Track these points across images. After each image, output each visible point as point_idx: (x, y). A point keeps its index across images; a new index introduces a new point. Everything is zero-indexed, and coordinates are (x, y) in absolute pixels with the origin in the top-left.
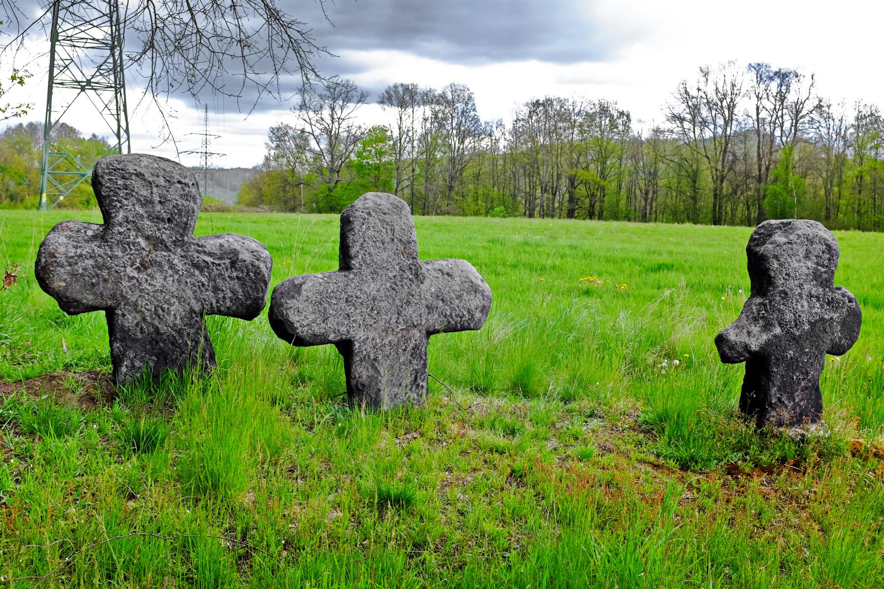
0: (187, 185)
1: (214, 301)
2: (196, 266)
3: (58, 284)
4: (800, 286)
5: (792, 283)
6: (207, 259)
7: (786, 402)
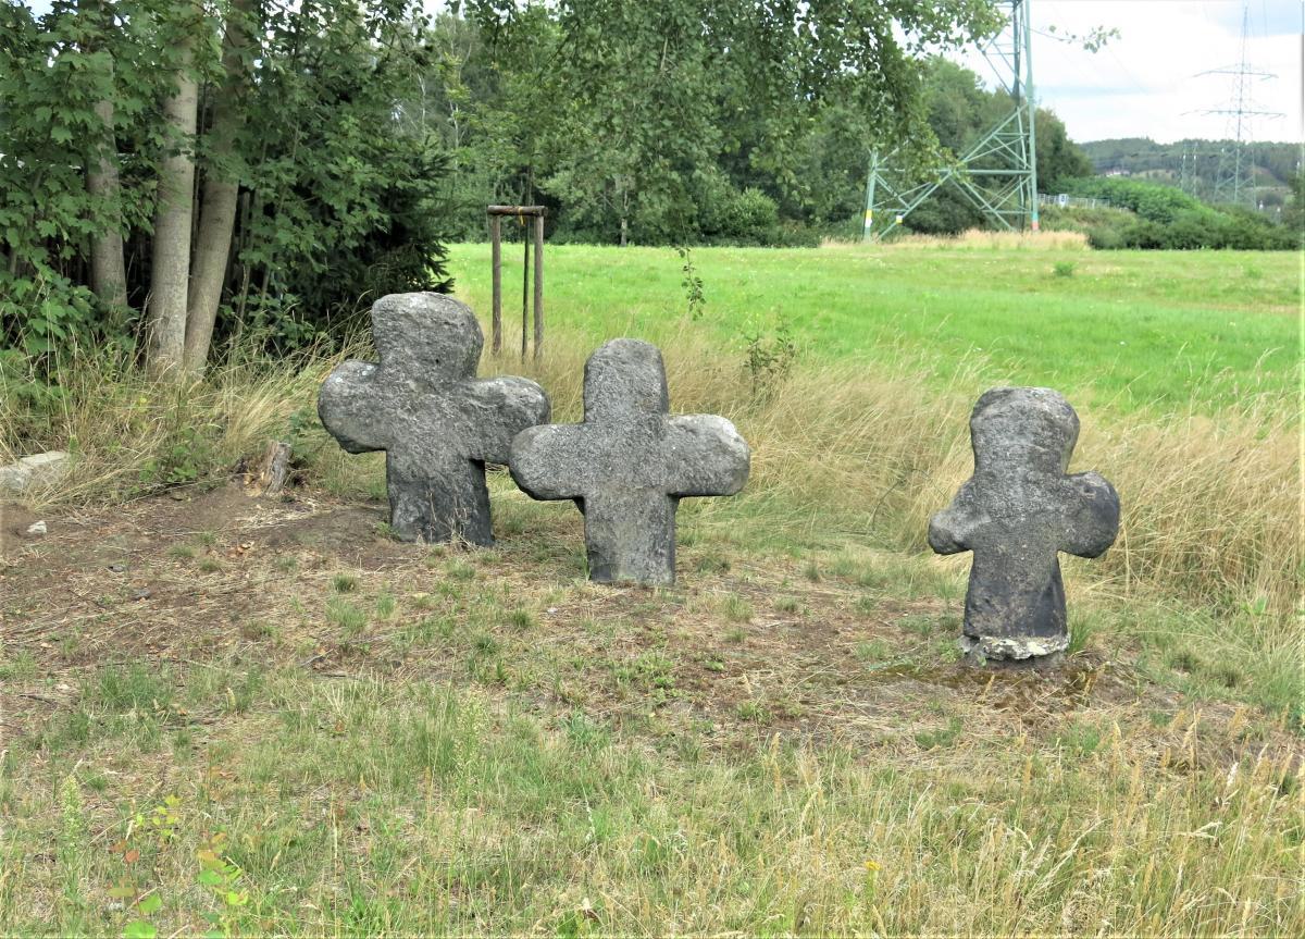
0: (455, 326)
1: (481, 447)
2: (464, 410)
3: (335, 424)
4: (1013, 468)
5: (1001, 464)
6: (475, 403)
7: (998, 607)
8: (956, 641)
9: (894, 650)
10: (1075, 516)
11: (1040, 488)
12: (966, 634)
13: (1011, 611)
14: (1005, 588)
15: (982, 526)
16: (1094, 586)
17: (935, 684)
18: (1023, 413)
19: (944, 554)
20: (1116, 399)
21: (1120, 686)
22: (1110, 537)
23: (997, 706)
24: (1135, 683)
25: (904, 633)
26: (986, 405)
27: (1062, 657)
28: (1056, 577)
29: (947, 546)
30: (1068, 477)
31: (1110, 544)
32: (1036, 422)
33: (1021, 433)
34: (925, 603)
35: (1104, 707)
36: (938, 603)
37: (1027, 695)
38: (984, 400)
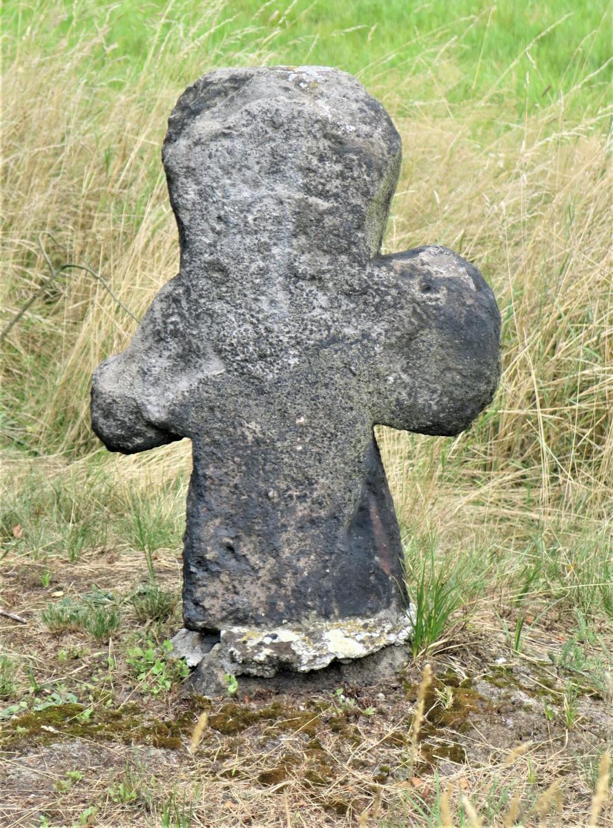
4: (263, 248)
5: (235, 243)
7: (254, 559)
8: (168, 644)
9: (34, 673)
10: (406, 344)
11: (322, 288)
12: (189, 626)
13: (285, 566)
14: (266, 514)
15: (204, 382)
16: (473, 494)
17: (128, 743)
18: (276, 126)
19: (127, 451)
20: (504, 78)
21: (528, 709)
22: (483, 387)
23: (266, 779)
24: (559, 702)
25: (57, 635)
26: (195, 113)
27: (400, 658)
28: (376, 481)
29: (130, 434)
30: (383, 260)
31: (482, 403)
32: (306, 144)
33: (274, 170)
34: (102, 564)
35: (497, 760)
36: (131, 560)
37: (328, 749)
38: (190, 101)
